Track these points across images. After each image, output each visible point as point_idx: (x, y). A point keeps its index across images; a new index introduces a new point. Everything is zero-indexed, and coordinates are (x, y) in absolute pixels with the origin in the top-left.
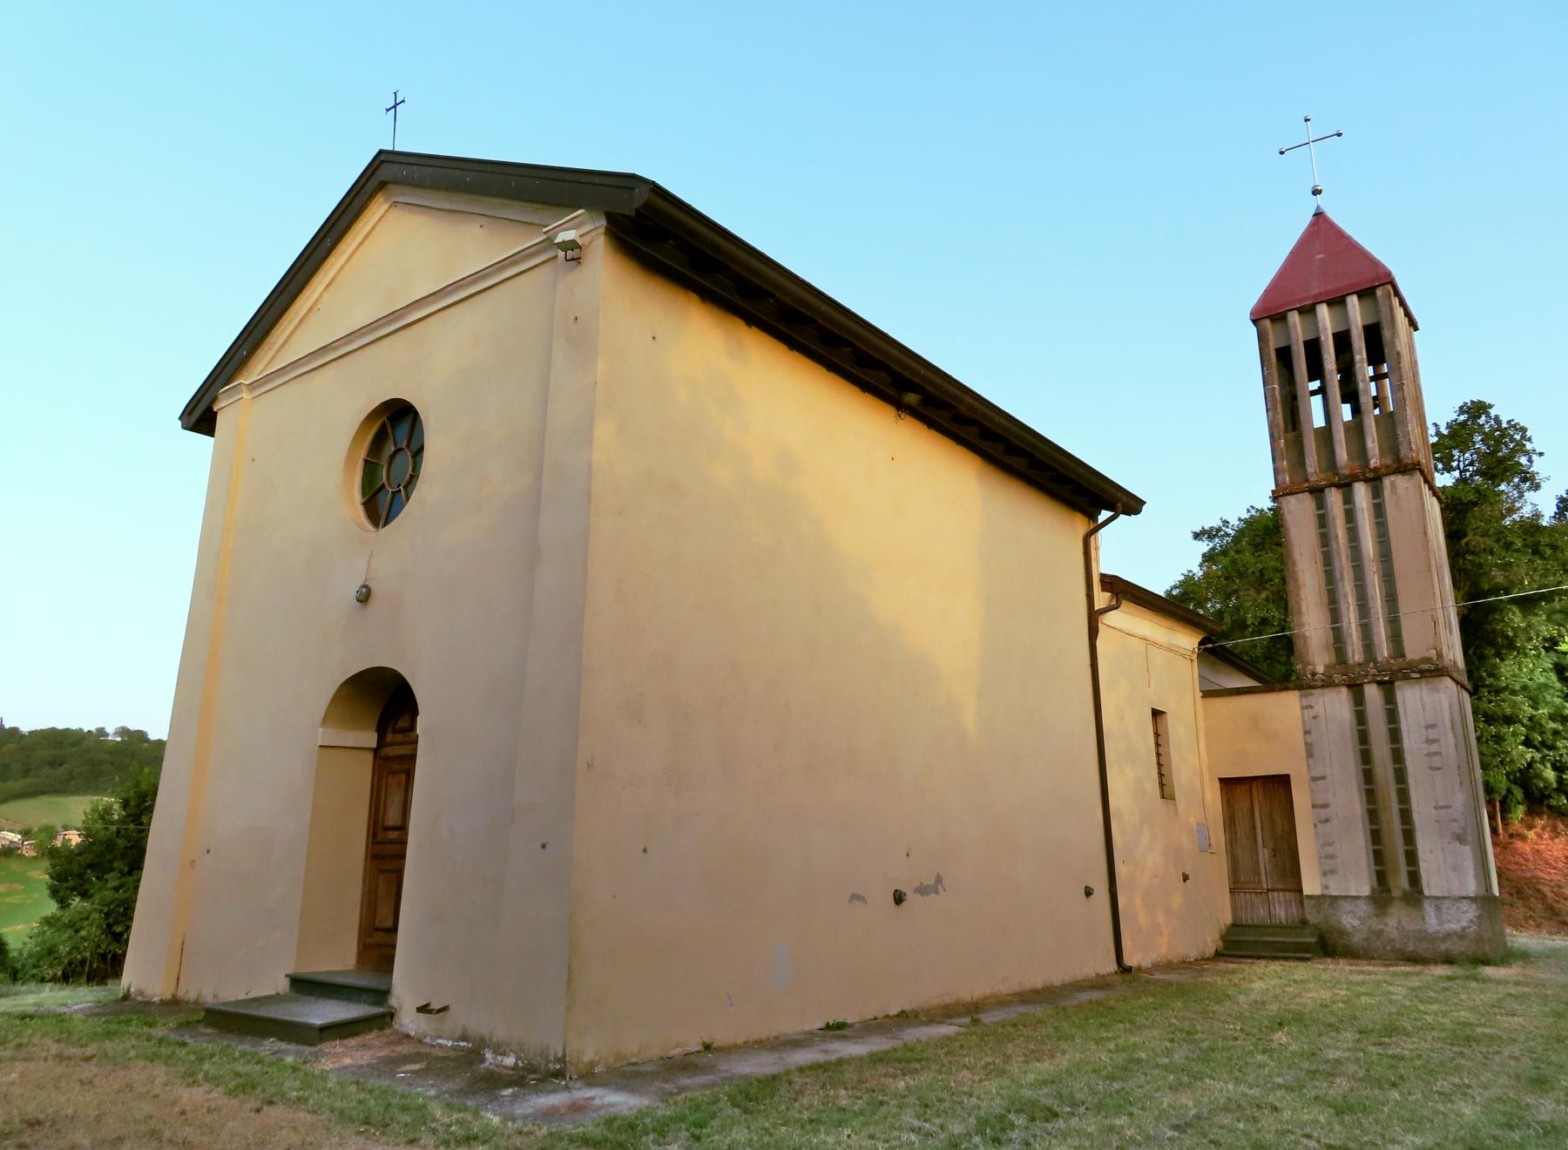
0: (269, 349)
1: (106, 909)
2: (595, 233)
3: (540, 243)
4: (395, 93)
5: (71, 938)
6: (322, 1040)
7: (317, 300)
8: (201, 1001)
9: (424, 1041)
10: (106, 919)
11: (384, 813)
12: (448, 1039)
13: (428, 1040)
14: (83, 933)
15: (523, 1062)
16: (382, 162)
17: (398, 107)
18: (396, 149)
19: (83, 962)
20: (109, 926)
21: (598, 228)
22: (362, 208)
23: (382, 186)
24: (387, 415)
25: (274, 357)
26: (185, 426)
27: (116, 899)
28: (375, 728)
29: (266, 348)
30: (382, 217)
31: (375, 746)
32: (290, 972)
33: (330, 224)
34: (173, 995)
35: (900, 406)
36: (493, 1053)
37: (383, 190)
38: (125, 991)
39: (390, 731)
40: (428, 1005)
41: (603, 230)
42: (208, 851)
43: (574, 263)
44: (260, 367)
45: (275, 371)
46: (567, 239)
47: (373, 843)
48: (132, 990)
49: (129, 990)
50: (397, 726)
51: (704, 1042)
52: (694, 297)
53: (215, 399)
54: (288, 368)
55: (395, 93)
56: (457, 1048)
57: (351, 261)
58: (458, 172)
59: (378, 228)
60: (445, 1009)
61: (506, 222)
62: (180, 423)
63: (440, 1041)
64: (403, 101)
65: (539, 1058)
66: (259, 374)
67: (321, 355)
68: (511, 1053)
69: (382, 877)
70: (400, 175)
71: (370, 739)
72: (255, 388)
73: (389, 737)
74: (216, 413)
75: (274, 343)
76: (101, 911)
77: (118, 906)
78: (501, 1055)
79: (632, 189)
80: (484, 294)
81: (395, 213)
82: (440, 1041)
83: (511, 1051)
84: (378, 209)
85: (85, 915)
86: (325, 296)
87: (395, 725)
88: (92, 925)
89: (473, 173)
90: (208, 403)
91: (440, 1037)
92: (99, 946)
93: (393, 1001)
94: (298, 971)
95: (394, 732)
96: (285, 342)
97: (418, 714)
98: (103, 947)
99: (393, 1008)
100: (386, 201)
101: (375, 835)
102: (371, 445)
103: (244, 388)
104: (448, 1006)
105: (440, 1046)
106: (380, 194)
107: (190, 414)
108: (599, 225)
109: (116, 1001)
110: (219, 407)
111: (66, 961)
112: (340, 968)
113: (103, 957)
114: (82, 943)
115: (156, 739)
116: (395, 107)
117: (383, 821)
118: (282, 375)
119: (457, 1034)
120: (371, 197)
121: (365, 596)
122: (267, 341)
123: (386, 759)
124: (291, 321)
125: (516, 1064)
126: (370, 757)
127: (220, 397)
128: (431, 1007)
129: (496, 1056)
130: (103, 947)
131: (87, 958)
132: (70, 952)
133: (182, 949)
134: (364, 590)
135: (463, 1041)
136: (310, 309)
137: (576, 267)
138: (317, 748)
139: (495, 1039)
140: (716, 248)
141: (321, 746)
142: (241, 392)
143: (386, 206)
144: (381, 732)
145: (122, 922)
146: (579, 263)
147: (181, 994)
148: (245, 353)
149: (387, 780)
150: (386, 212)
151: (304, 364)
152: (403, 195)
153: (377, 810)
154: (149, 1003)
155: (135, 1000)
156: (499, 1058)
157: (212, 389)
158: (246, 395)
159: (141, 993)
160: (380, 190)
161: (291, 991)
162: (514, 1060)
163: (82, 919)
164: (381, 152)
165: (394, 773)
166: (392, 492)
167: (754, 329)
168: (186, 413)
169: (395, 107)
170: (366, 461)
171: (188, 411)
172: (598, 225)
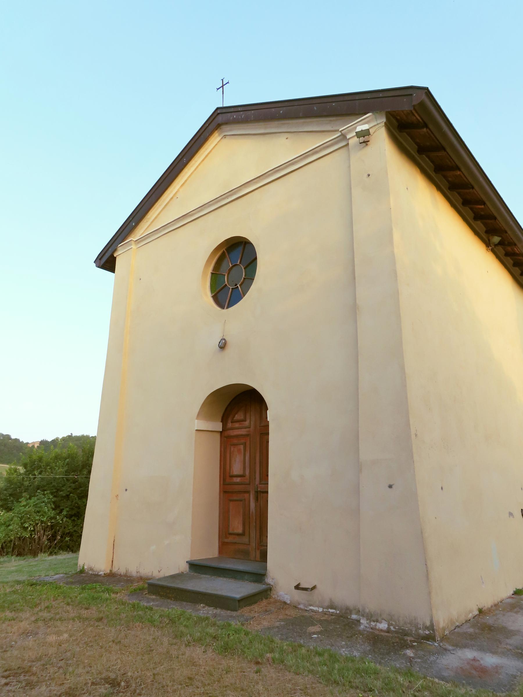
0: (147, 221)
1: (20, 516)
2: (379, 125)
3: (335, 138)
4: (222, 80)
5: (5, 530)
6: (240, 607)
7: (176, 193)
8: (128, 575)
9: (299, 607)
10: (21, 520)
11: (230, 467)
12: (318, 607)
13: (301, 606)
14: (11, 527)
15: (394, 628)
16: (218, 114)
17: (224, 87)
18: (224, 106)
19: (11, 541)
20: (22, 524)
21: (380, 123)
22: (206, 140)
23: (219, 126)
24: (225, 248)
25: (149, 225)
26: (98, 266)
27: (25, 511)
28: (220, 420)
29: (145, 221)
30: (216, 145)
31: (221, 430)
32: (188, 560)
33: (187, 149)
34: (111, 571)
35: (487, 243)
36: (367, 620)
37: (219, 129)
38: (81, 568)
39: (229, 421)
40: (299, 584)
41: (383, 124)
42: (126, 490)
43: (364, 144)
44: (142, 232)
45: (154, 231)
46: (363, 129)
47: (224, 484)
48: (85, 567)
49: (83, 567)
50: (235, 419)
51: (479, 609)
52: (419, 170)
53: (115, 250)
54: (261, 178)
55: (222, 80)
56: (327, 613)
57: (196, 170)
58: (273, 110)
59: (213, 151)
60: (314, 588)
61: (306, 133)
62: (95, 264)
63: (312, 608)
64: (218, 89)
65: (409, 625)
66: (140, 236)
67: (155, 234)
68: (383, 621)
69: (231, 504)
70: (231, 118)
71: (219, 427)
72: (139, 243)
73: (230, 425)
74: (115, 258)
75: (149, 219)
76: (18, 517)
77: (26, 514)
78: (374, 621)
79: (411, 95)
80: (148, 244)
81: (225, 141)
82: (312, 608)
83: (383, 619)
84: (215, 139)
85: (10, 518)
86: (181, 190)
87: (234, 417)
88: (14, 523)
89: (284, 108)
90: (111, 253)
91: (311, 605)
92: (17, 534)
93: (269, 580)
94: (193, 559)
95: (232, 422)
96: (156, 218)
97: (268, 409)
98: (19, 534)
99: (270, 584)
100: (219, 135)
101: (224, 480)
102: (215, 265)
103: (133, 242)
104: (316, 585)
105: (312, 611)
106: (216, 131)
107: (100, 259)
108: (381, 121)
109: (76, 573)
110: (117, 254)
111: (3, 541)
112: (211, 557)
113: (19, 538)
114: (10, 532)
115: (15, 438)
116: (223, 86)
117: (230, 473)
118: (257, 183)
119: (326, 604)
120: (211, 133)
121: (223, 346)
122: (146, 217)
123: (229, 437)
124: (160, 205)
125: (389, 628)
126: (218, 436)
127: (119, 249)
128: (301, 587)
129: (370, 622)
130: (19, 534)
131: (12, 539)
132: (4, 537)
133: (114, 544)
134: (224, 341)
135: (331, 609)
136: (172, 198)
137: (365, 146)
138: (195, 431)
139: (367, 611)
140: (444, 135)
141: (196, 430)
142: (131, 245)
143: (219, 138)
144: (224, 420)
145: (27, 522)
146: (367, 145)
147: (115, 570)
148: (134, 224)
149: (230, 449)
150: (218, 142)
151: (170, 226)
152: (231, 130)
153: (225, 465)
154: (97, 575)
155: (88, 573)
156: (373, 624)
157: (114, 245)
158: (134, 246)
159: (91, 569)
160: (216, 130)
161: (189, 571)
162: (386, 626)
163: (9, 521)
164: (218, 109)
165: (235, 445)
166: (232, 288)
167: (439, 192)
168: (98, 259)
169: (223, 86)
170: (212, 273)
171: (100, 257)
172: (379, 122)
